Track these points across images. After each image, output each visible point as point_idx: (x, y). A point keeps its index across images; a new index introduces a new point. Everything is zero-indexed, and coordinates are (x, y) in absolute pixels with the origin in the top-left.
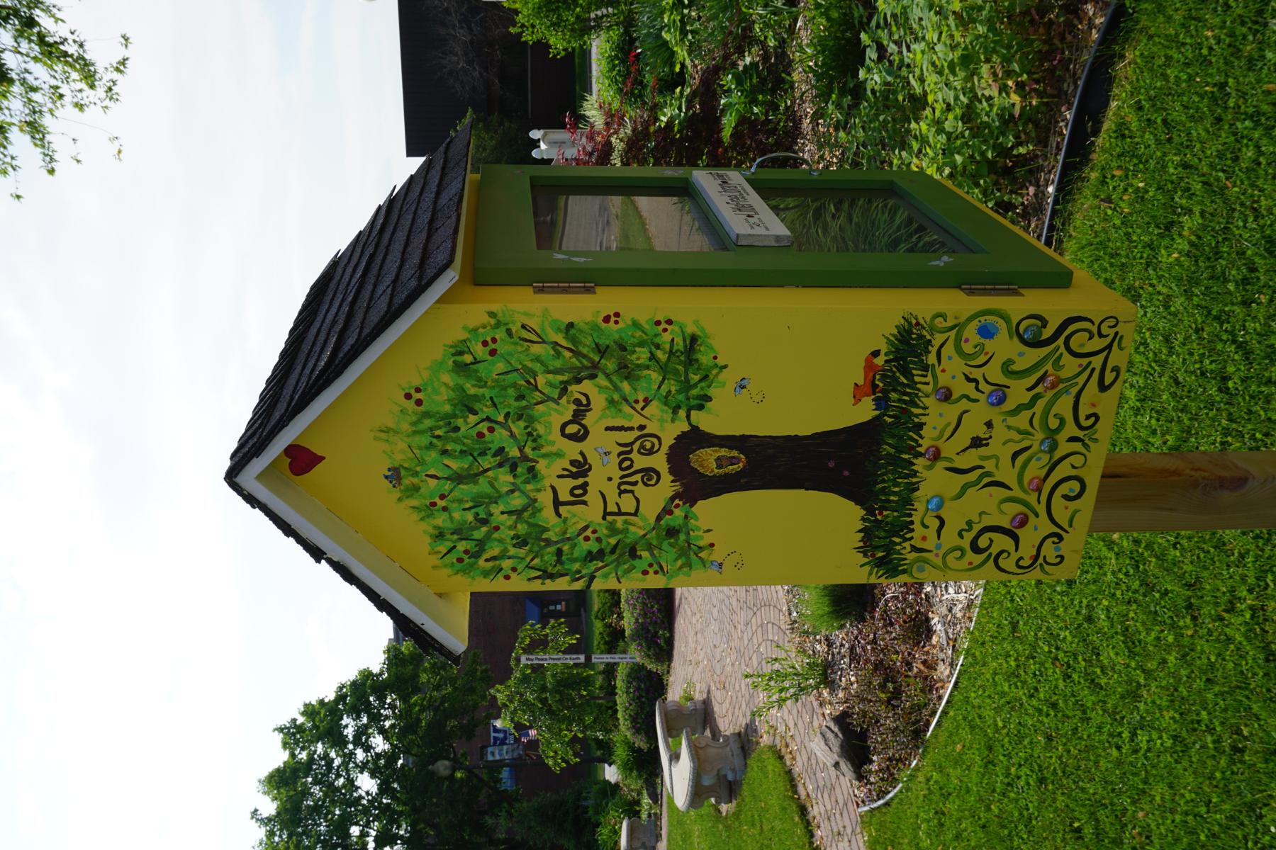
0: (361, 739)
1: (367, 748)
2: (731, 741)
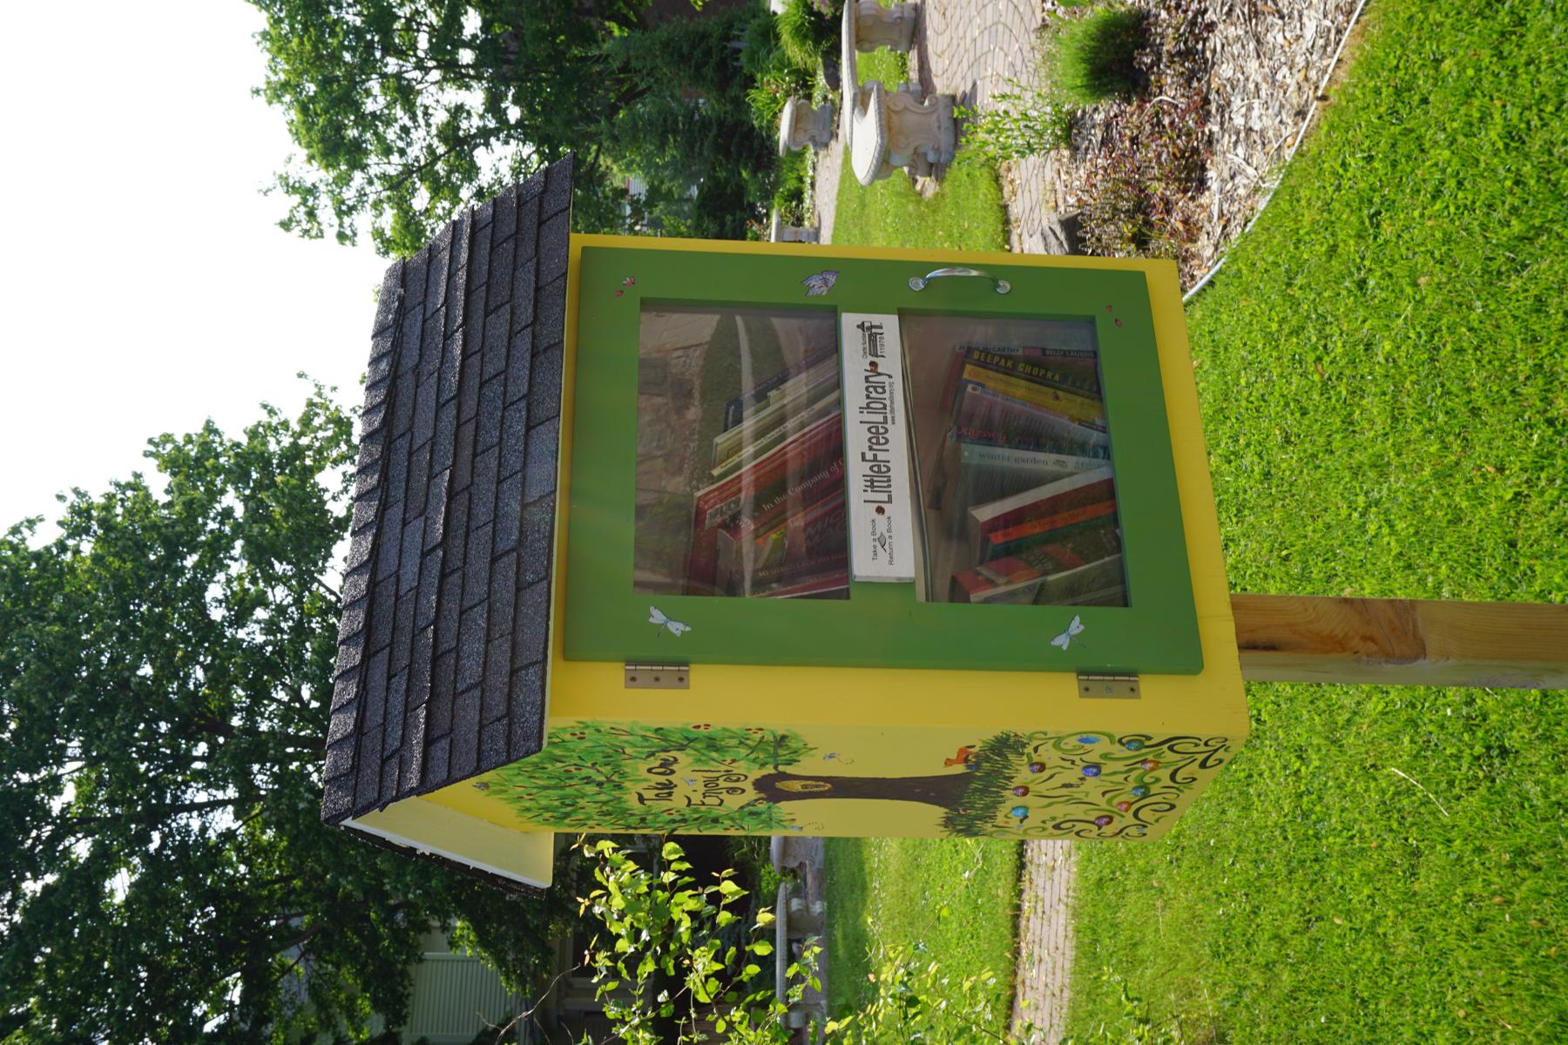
2: (941, 105)
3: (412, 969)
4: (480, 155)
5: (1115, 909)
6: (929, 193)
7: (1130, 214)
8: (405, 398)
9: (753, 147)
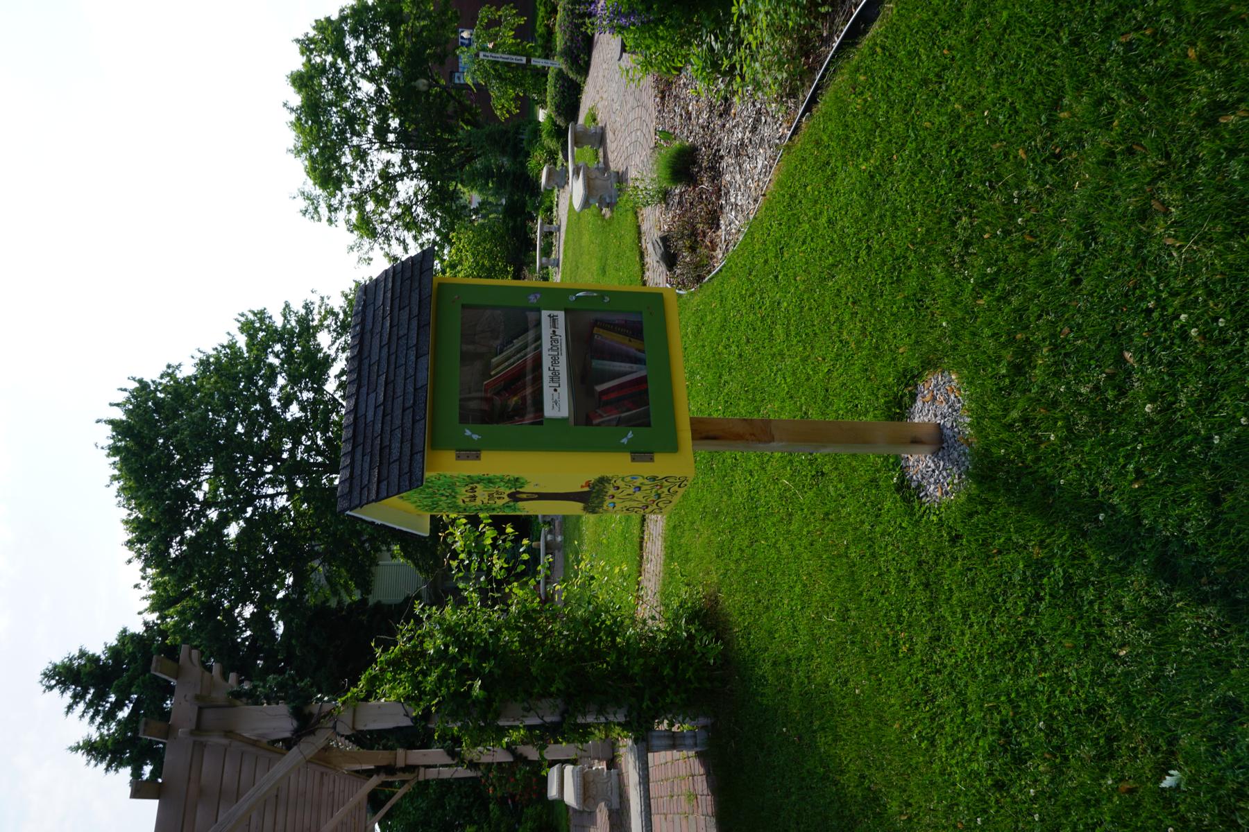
0: (361, 54)
1: (365, 61)
3: (373, 569)
4: (399, 185)
5: (680, 538)
6: (608, 216)
7: (689, 236)
8: (367, 343)
9: (529, 185)
